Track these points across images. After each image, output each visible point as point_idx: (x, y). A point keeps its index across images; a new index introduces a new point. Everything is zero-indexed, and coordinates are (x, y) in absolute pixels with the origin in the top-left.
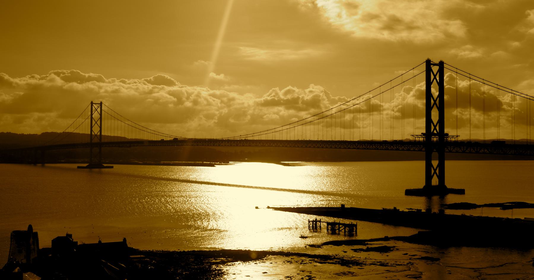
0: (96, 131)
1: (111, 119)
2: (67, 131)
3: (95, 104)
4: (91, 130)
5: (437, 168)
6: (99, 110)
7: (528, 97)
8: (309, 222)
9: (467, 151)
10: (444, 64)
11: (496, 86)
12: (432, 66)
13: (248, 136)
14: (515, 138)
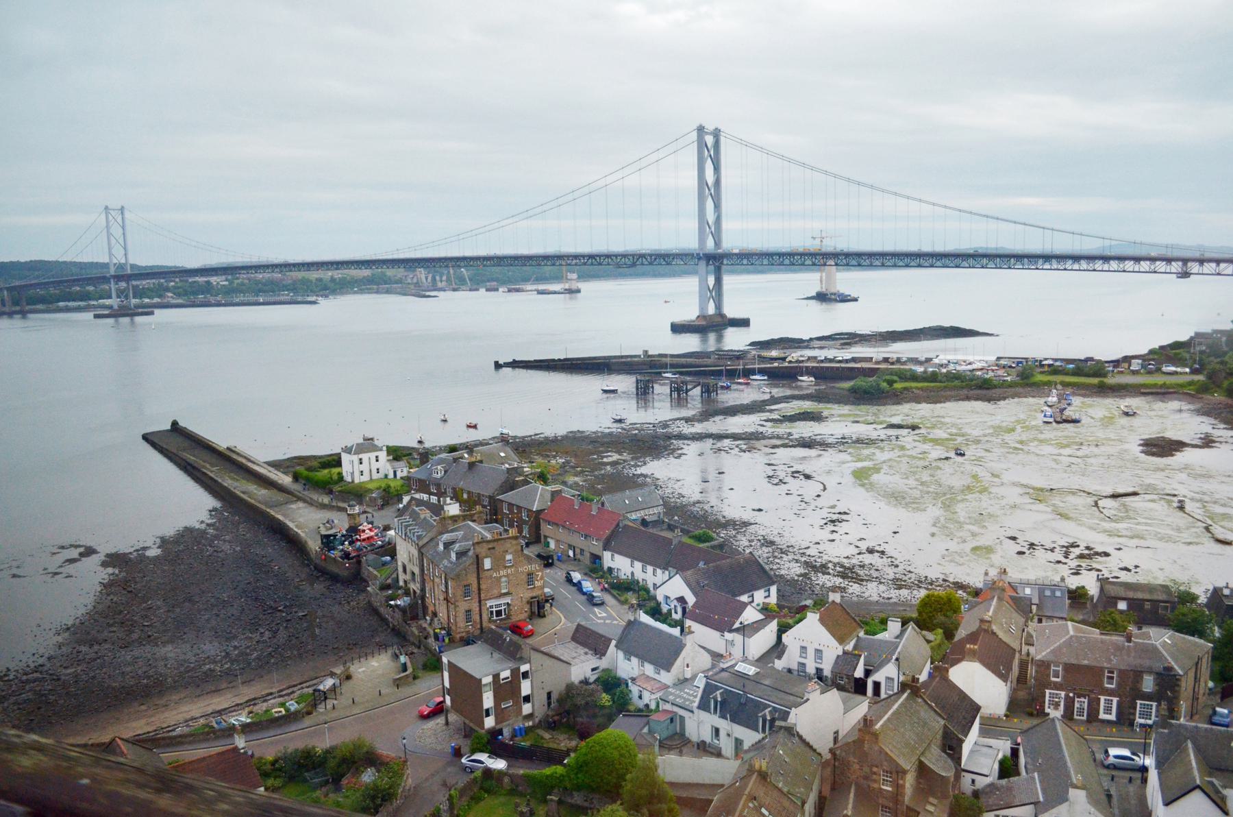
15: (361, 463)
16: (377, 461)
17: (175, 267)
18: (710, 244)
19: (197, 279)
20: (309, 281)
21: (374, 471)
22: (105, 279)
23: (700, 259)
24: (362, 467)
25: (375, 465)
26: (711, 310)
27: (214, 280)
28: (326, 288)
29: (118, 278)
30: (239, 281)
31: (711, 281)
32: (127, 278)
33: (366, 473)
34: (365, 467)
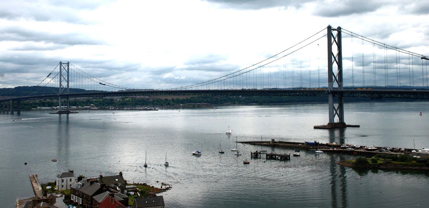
0: (64, 84)
1: (423, 79)
2: (39, 85)
3: (64, 64)
4: (61, 84)
5: (337, 109)
6: (66, 68)
7: (374, 42)
8: (252, 153)
9: (351, 96)
10: (342, 29)
11: (372, 41)
12: (332, 31)
13: (188, 87)
14: (376, 85)
15: (63, 182)
16: (71, 181)
17: (134, 90)
18: (336, 85)
19: (106, 98)
20: (162, 100)
21: (69, 186)
22: (56, 97)
23: (329, 93)
24: (63, 184)
25: (69, 183)
26: (336, 119)
27: (115, 98)
28: (169, 104)
29: (62, 96)
30: (127, 99)
31: (336, 106)
32: (67, 96)
33: (65, 186)
34: (64, 184)
